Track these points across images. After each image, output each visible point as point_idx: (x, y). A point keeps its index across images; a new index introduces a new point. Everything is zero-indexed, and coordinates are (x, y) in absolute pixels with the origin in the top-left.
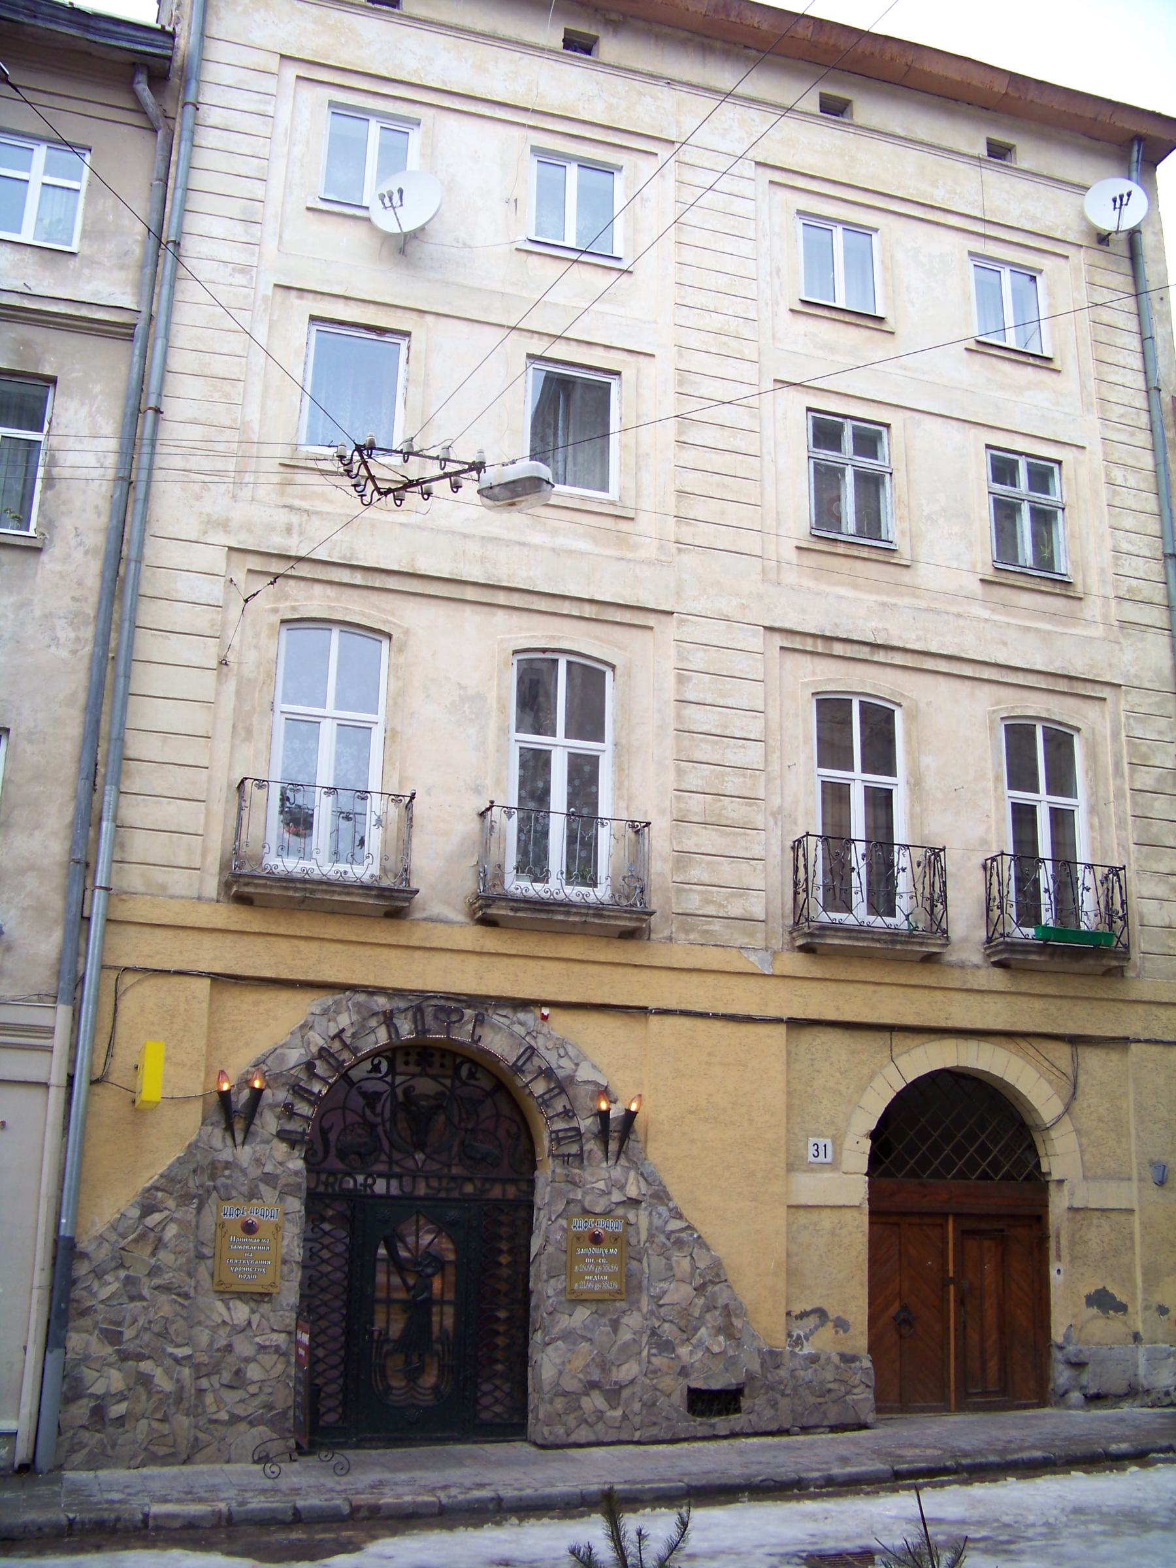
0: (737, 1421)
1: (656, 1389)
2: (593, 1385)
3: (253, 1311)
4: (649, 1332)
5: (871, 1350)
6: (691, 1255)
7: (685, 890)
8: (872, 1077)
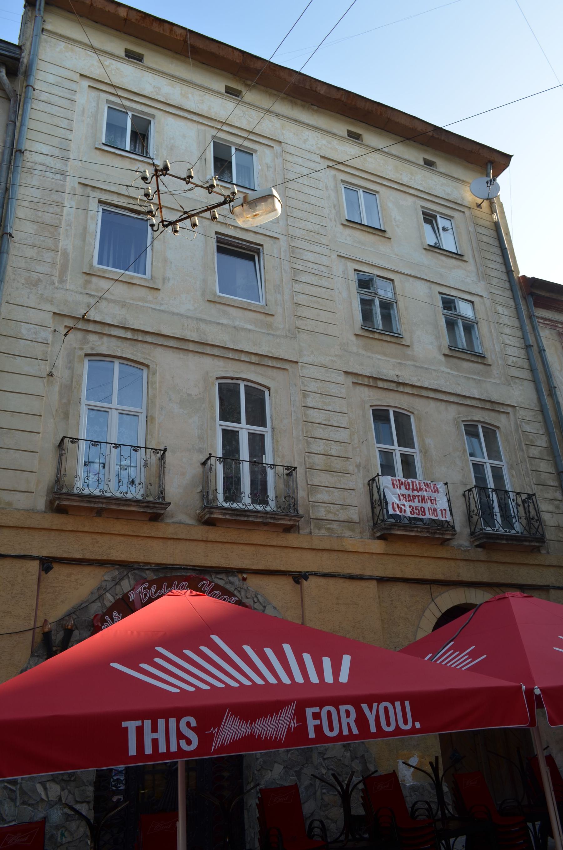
3: (63, 789)
7: (317, 506)
8: (424, 611)
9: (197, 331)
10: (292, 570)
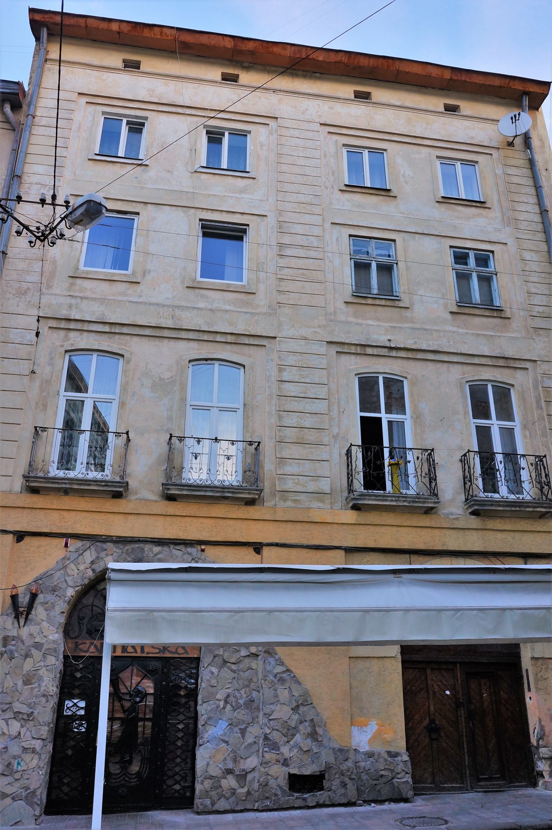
0: (321, 796)
1: (268, 774)
2: (229, 772)
3: (22, 726)
4: (263, 737)
5: (408, 749)
6: (289, 687)
7: (284, 478)
9: (172, 318)
10: (252, 541)
